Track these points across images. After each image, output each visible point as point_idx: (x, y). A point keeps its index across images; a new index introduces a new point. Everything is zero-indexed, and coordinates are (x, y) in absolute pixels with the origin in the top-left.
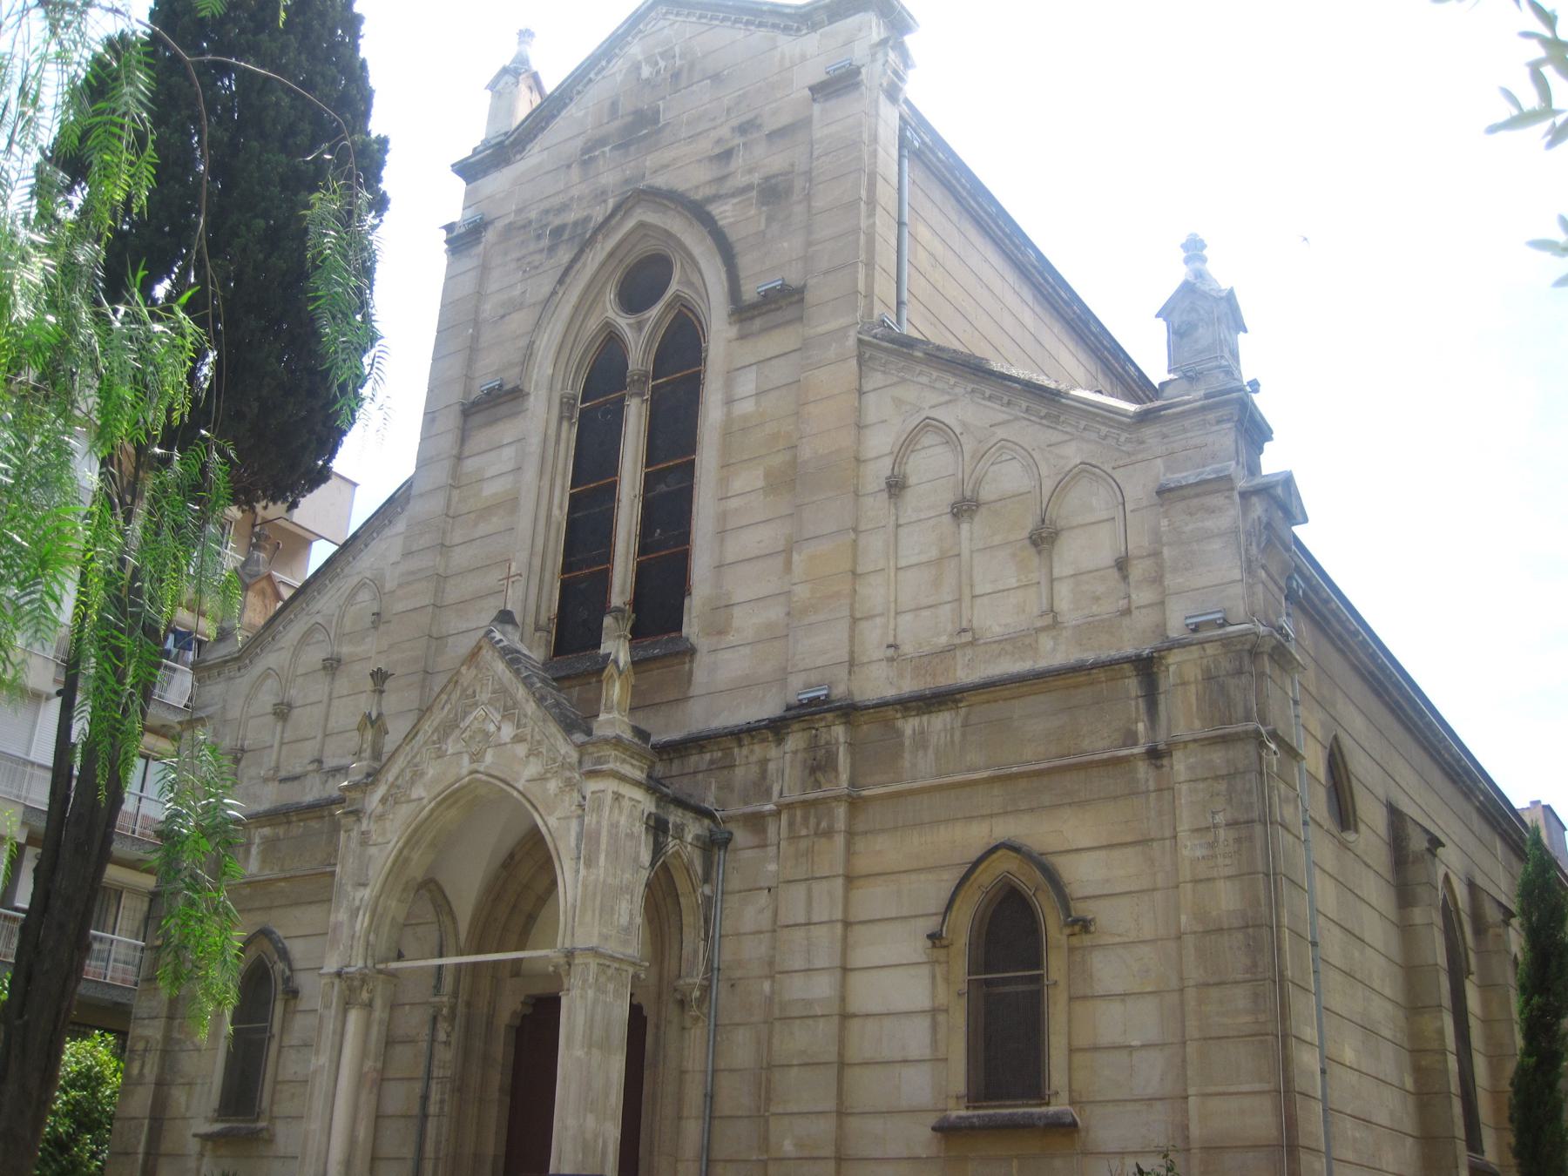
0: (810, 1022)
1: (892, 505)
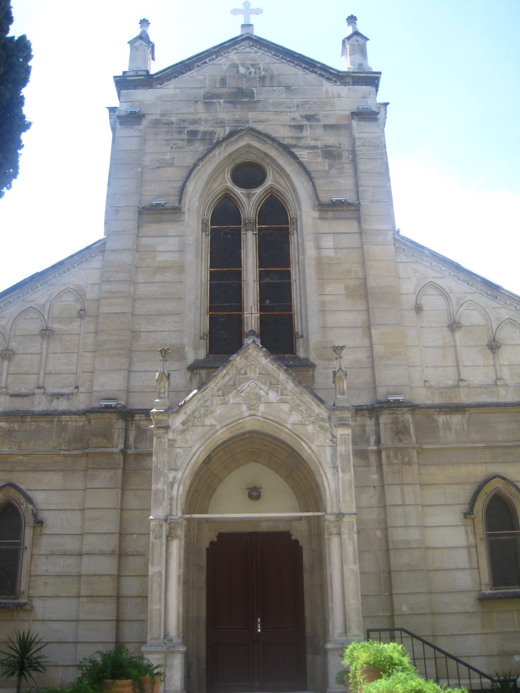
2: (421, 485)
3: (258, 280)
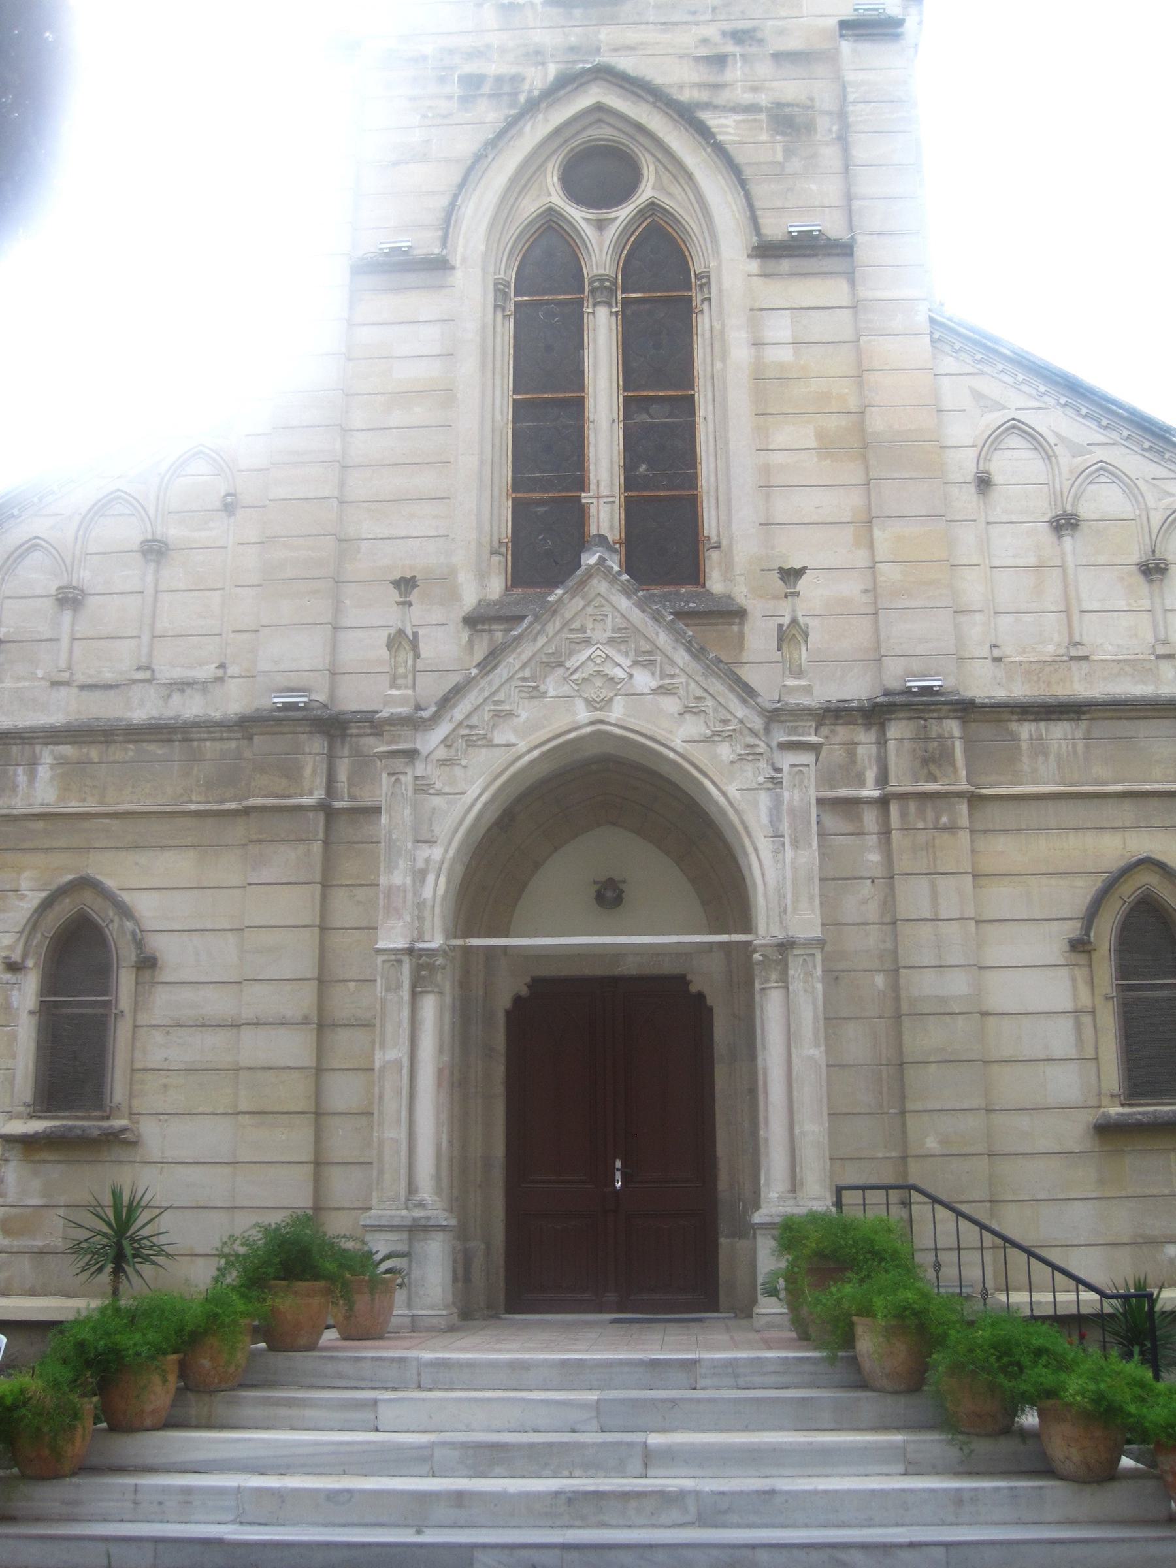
0: (947, 1019)
1: (981, 502)
2: (976, 876)
3: (621, 418)
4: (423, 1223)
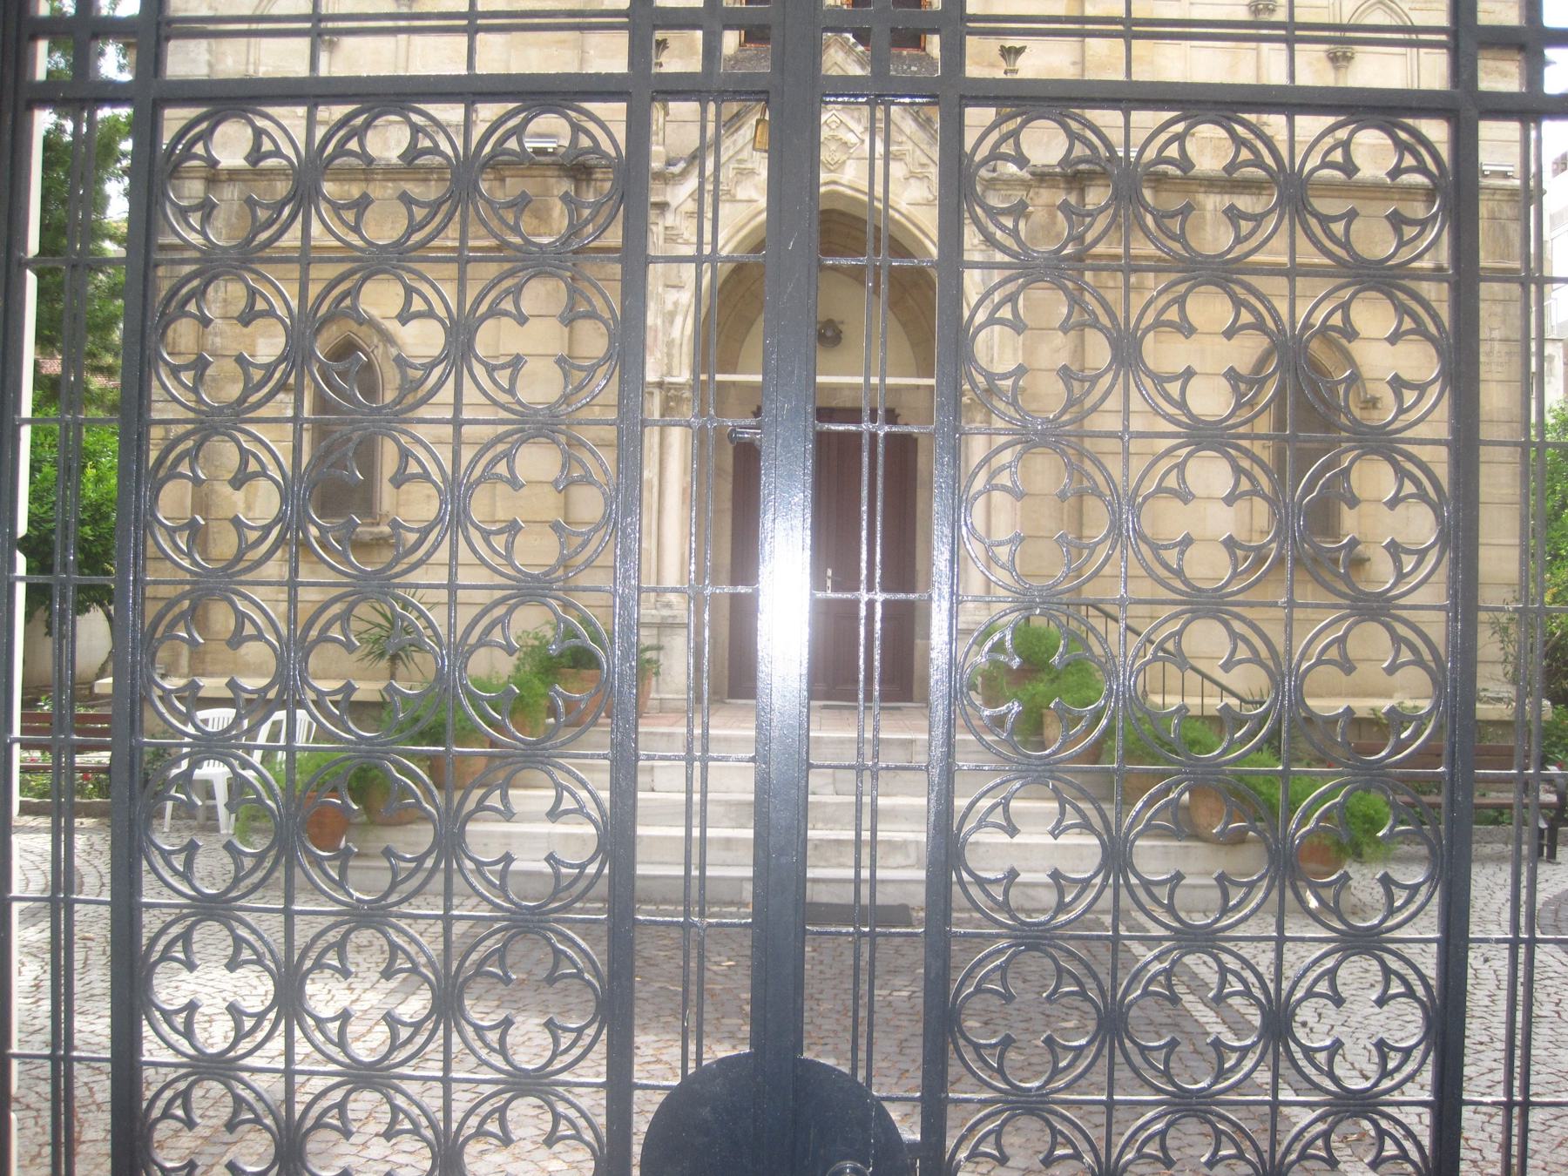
4: (670, 621)
